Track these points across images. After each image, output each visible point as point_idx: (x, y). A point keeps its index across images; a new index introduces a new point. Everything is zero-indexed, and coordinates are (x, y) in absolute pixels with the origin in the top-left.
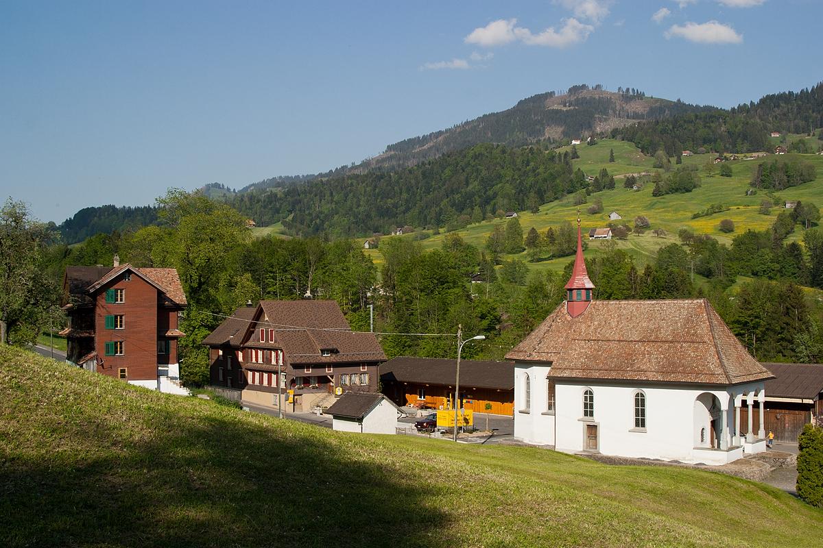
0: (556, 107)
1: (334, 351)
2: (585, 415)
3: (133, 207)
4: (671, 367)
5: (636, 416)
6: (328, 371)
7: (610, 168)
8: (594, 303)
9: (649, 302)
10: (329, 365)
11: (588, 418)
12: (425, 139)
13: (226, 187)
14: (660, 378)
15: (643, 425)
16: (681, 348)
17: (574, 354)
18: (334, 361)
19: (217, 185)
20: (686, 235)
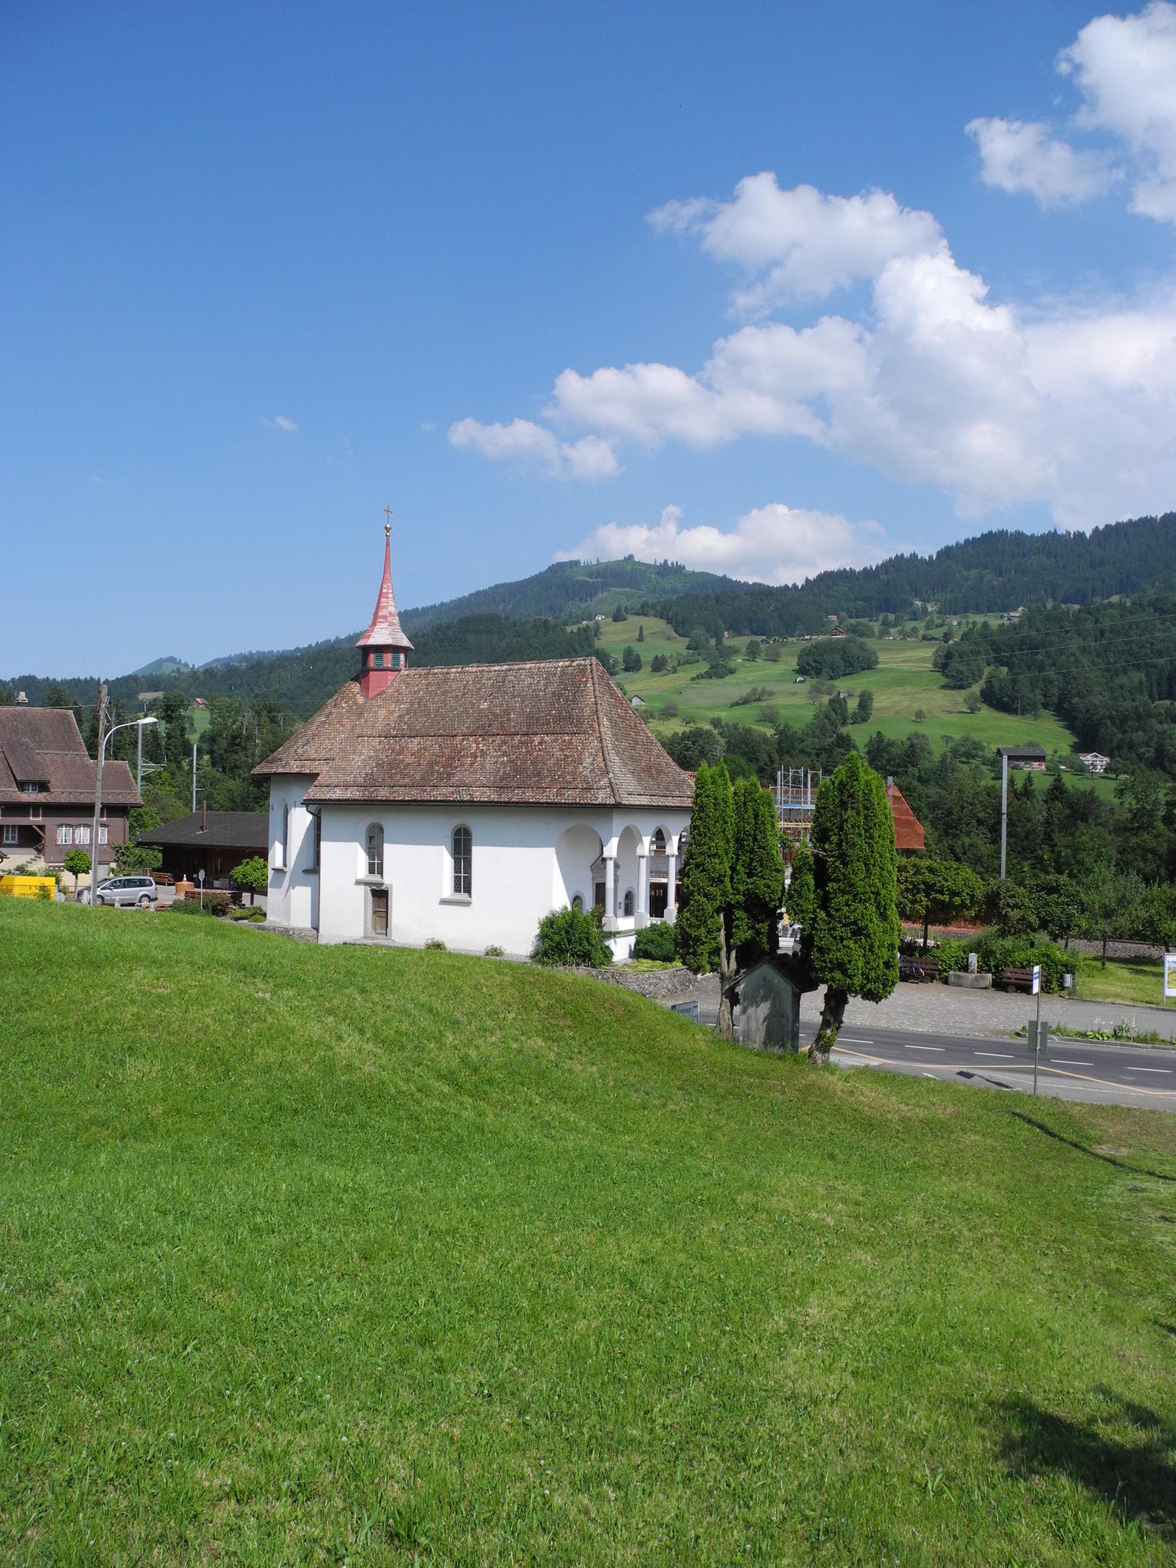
0: (581, 578)
1: (43, 786)
2: (370, 873)
3: (59, 679)
4: (516, 774)
5: (456, 872)
6: (33, 820)
7: (638, 648)
8: (406, 672)
9: (497, 668)
10: (35, 808)
11: (375, 878)
12: (425, 611)
13: (183, 662)
14: (494, 797)
15: (468, 890)
16: (540, 743)
17: (358, 760)
18: (44, 801)
19: (171, 659)
20: (716, 723)
